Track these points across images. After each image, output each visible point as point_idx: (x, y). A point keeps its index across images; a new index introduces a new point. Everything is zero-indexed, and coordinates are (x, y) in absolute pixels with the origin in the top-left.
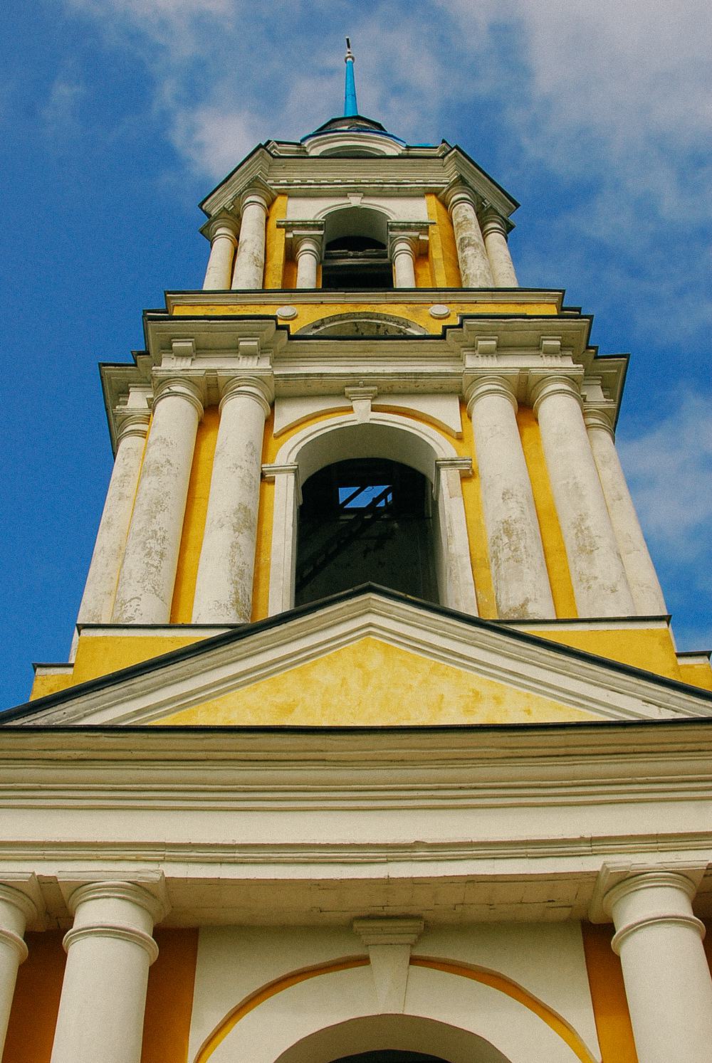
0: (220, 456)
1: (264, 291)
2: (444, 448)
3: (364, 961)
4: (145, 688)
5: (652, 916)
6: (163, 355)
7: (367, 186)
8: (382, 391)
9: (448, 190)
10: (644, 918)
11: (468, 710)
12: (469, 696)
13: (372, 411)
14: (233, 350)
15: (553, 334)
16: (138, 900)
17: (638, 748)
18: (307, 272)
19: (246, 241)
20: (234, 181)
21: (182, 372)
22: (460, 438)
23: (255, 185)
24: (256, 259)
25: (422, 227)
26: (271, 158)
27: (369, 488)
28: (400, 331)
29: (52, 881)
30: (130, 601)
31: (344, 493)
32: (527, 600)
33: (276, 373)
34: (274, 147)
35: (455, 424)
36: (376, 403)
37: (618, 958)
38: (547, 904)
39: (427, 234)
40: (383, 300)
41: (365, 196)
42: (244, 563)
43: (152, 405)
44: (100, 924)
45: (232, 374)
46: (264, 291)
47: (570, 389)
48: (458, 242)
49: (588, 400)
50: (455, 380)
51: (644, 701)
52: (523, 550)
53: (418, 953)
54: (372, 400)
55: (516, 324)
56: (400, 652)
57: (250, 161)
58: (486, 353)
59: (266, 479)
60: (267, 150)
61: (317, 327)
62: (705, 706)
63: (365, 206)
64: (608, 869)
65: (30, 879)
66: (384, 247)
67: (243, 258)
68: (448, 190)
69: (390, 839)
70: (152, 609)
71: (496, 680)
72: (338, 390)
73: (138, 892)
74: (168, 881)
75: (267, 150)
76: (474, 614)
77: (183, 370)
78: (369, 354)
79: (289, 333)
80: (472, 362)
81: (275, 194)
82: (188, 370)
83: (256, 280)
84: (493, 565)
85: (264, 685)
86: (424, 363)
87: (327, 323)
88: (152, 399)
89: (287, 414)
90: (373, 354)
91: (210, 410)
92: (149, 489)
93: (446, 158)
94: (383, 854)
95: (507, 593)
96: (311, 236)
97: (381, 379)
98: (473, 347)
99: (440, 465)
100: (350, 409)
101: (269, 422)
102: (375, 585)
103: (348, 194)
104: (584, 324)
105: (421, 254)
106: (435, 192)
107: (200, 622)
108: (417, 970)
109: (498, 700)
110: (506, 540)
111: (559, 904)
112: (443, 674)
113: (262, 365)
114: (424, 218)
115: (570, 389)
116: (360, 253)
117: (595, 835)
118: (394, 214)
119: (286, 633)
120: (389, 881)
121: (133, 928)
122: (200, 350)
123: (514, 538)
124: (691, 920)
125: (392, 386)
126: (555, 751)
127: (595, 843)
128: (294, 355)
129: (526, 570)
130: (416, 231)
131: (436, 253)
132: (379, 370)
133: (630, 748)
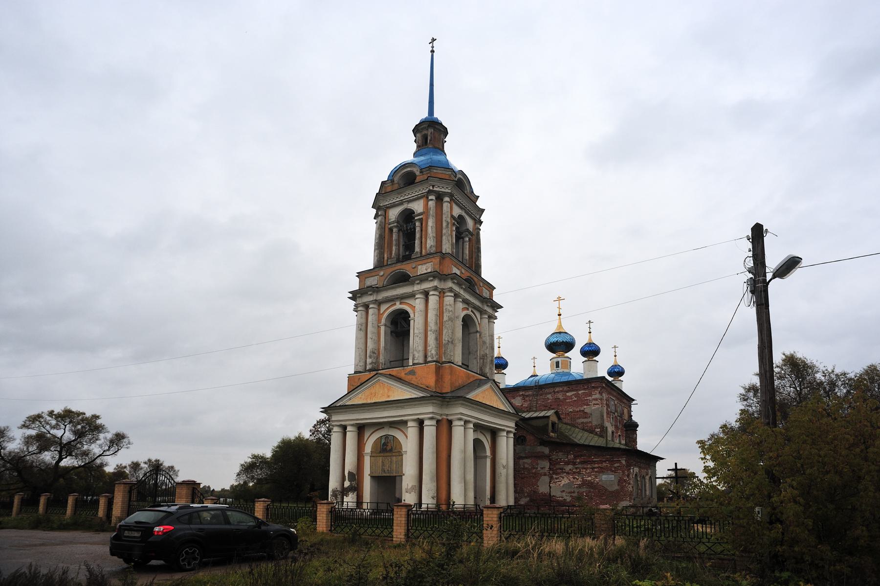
3: (383, 428)
15: (430, 276)
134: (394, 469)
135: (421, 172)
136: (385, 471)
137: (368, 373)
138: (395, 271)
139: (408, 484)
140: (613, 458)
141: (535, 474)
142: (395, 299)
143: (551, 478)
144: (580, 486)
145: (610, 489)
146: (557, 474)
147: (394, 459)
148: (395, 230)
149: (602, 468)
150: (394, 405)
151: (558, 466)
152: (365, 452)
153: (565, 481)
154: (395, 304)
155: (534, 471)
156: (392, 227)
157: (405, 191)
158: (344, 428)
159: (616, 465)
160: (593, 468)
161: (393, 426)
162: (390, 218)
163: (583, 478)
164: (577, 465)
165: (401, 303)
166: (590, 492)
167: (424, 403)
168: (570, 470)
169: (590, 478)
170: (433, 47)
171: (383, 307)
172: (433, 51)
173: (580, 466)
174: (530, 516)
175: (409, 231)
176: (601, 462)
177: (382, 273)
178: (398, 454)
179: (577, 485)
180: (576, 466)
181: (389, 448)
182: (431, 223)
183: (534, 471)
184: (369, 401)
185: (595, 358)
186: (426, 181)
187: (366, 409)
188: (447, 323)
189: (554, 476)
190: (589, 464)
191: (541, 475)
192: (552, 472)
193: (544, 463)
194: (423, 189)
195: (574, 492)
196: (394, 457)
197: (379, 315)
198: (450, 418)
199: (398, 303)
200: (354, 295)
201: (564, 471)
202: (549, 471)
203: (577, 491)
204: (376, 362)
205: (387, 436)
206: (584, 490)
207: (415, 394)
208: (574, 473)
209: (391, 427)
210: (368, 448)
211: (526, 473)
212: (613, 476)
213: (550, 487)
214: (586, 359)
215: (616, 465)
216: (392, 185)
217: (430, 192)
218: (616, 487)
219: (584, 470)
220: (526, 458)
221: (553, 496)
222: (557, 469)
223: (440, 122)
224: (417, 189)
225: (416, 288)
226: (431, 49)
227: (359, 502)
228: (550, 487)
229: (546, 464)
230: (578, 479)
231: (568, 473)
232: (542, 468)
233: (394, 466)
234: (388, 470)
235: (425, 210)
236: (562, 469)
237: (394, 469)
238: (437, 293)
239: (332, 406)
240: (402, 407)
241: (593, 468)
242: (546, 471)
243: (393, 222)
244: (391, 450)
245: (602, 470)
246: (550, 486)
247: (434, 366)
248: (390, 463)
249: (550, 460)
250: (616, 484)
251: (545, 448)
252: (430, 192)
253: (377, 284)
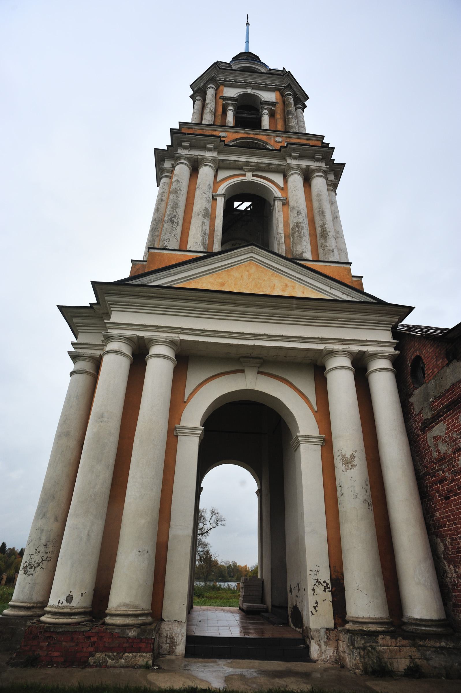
0: (198, 189)
1: (214, 125)
2: (277, 193)
3: (242, 371)
4: (174, 273)
5: (339, 366)
6: (178, 148)
7: (254, 85)
8: (257, 169)
9: (284, 90)
10: (336, 366)
11: (283, 290)
12: (283, 285)
13: (252, 176)
14: (204, 148)
15: (319, 153)
16: (171, 346)
17: (340, 309)
18: (230, 117)
19: (208, 103)
20: (204, 77)
21: (185, 155)
22: (282, 189)
23: (212, 80)
24: (212, 111)
25: (273, 104)
26: (219, 69)
27: (245, 203)
28: (264, 146)
29: (142, 338)
30: (166, 240)
31: (236, 204)
32: (303, 252)
33: (219, 158)
34: (219, 64)
35: (281, 184)
36: (254, 173)
37: (326, 378)
38: (305, 358)
39: (275, 107)
40: (258, 133)
41: (253, 89)
42: (206, 229)
43: (174, 167)
44: (159, 353)
45: (203, 157)
46: (214, 125)
47: (323, 175)
48: (286, 112)
49: (329, 180)
50: (283, 167)
51: (342, 293)
52: (303, 234)
53: (261, 370)
54: (253, 172)
55: (306, 148)
56: (261, 267)
57: (211, 69)
58: (295, 158)
59: (214, 199)
60: (217, 65)
61: (234, 142)
62: (362, 297)
63: (253, 93)
64: (326, 349)
65: (135, 337)
66: (258, 111)
67: (207, 110)
68: (284, 90)
69: (252, 332)
70: (174, 244)
71: (293, 281)
72: (240, 167)
73: (171, 343)
74: (182, 341)
75: (217, 65)
76: (284, 255)
77: (186, 154)
78: (252, 154)
79: (224, 143)
80: (289, 161)
81: (219, 84)
82: (187, 154)
83: (211, 120)
84: (291, 238)
85: (215, 275)
86: (272, 160)
87: (238, 140)
88: (173, 164)
89: (222, 175)
90: (254, 154)
91: (194, 171)
92: (173, 199)
93: (285, 76)
94: (253, 337)
95: (296, 249)
96: (232, 104)
97: (256, 164)
98: (290, 156)
99: (275, 199)
100: (244, 175)
101: (216, 176)
102: (255, 243)
103: (247, 87)
104: (331, 151)
105: (272, 115)
106: (279, 90)
107: (191, 249)
108: (260, 375)
109: (293, 287)
110: (297, 229)
111: (307, 358)
112: (275, 277)
113: (213, 155)
114: (274, 100)
115: (323, 175)
116: (249, 112)
117: (323, 337)
118: (263, 97)
119: (223, 257)
120: (254, 346)
121: (170, 356)
122: (192, 147)
123: (300, 229)
124: (352, 368)
125: (260, 167)
126: (312, 307)
127: (322, 340)
128: (225, 152)
129: (303, 241)
130: (271, 106)
131: (278, 116)
132: (256, 161)
133: (337, 309)
152: (183, 423)
165: (253, 175)
167: (273, 315)
209: (259, 372)
220: (435, 419)
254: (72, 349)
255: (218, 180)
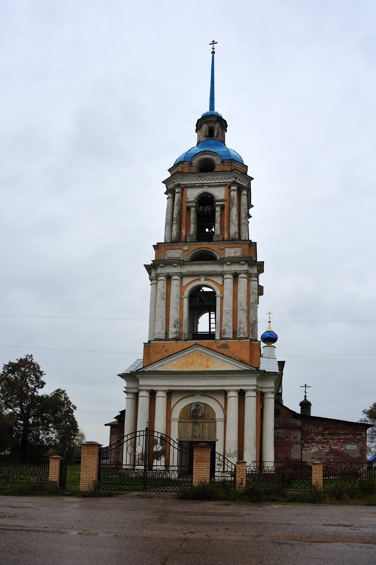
3: (195, 395)
15: (243, 261)
100: (200, 280)
134: (206, 435)
135: (223, 162)
136: (195, 436)
137: (174, 342)
138: (201, 248)
139: (230, 449)
140: (356, 431)
141: (288, 442)
142: (201, 274)
143: (303, 446)
144: (328, 454)
145: (353, 456)
146: (308, 443)
147: (206, 425)
148: (193, 209)
149: (347, 439)
150: (217, 375)
151: (309, 437)
152: (172, 417)
153: (315, 449)
154: (200, 280)
155: (287, 440)
156: (191, 206)
157: (206, 176)
158: (153, 394)
159: (358, 437)
160: (339, 439)
161: (204, 394)
162: (187, 197)
163: (330, 447)
164: (326, 436)
165: (205, 280)
166: (336, 458)
167: (250, 376)
168: (320, 440)
169: (336, 447)
170: (213, 48)
171: (186, 281)
172: (213, 53)
173: (328, 437)
174: (106, 471)
175: (205, 213)
176: (346, 434)
177: (186, 248)
178: (210, 421)
179: (325, 452)
180: (325, 437)
181: (200, 415)
182: (234, 211)
183: (287, 440)
184: (185, 369)
185: (273, 345)
186: (231, 172)
187: (217, 377)
188: (254, 305)
189: (306, 445)
190: (336, 435)
191: (294, 443)
192: (304, 441)
193: (296, 433)
194: (225, 178)
195: (323, 459)
196: (207, 424)
197: (182, 288)
198: (264, 391)
199: (203, 279)
200: (148, 268)
201: (314, 440)
202: (301, 440)
203: (325, 457)
204: (180, 333)
205: (197, 404)
206: (332, 457)
207: (238, 367)
208: (323, 442)
209: (201, 395)
210: (176, 414)
211: (280, 441)
212: (356, 446)
213: (302, 454)
214: (265, 345)
215: (358, 437)
216: (190, 166)
217: (234, 183)
218: (358, 455)
219: (332, 441)
221: (304, 462)
222: (308, 439)
223: (220, 116)
224: (219, 177)
225: (226, 268)
226: (212, 50)
227: (167, 465)
228: (302, 454)
229: (299, 435)
230: (326, 448)
231: (317, 443)
232: (295, 438)
233: (207, 432)
234: (199, 436)
235: (227, 198)
236: (312, 439)
237: (206, 435)
238: (246, 276)
239: (138, 371)
240: (224, 378)
241: (339, 439)
242: (298, 441)
243: (192, 202)
244: (203, 417)
245: (347, 441)
246: (301, 453)
247: (249, 343)
248: (201, 429)
249: (302, 431)
250: (358, 452)
251: (298, 420)
252: (234, 183)
253: (180, 258)
254: (125, 390)
255: (184, 285)
